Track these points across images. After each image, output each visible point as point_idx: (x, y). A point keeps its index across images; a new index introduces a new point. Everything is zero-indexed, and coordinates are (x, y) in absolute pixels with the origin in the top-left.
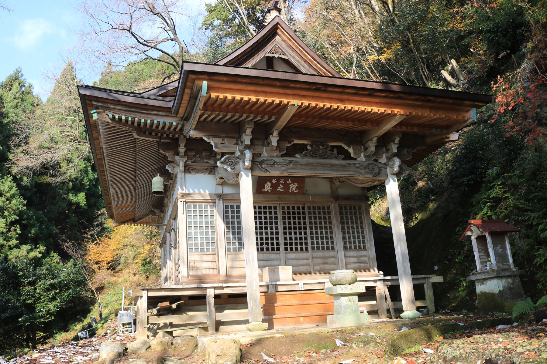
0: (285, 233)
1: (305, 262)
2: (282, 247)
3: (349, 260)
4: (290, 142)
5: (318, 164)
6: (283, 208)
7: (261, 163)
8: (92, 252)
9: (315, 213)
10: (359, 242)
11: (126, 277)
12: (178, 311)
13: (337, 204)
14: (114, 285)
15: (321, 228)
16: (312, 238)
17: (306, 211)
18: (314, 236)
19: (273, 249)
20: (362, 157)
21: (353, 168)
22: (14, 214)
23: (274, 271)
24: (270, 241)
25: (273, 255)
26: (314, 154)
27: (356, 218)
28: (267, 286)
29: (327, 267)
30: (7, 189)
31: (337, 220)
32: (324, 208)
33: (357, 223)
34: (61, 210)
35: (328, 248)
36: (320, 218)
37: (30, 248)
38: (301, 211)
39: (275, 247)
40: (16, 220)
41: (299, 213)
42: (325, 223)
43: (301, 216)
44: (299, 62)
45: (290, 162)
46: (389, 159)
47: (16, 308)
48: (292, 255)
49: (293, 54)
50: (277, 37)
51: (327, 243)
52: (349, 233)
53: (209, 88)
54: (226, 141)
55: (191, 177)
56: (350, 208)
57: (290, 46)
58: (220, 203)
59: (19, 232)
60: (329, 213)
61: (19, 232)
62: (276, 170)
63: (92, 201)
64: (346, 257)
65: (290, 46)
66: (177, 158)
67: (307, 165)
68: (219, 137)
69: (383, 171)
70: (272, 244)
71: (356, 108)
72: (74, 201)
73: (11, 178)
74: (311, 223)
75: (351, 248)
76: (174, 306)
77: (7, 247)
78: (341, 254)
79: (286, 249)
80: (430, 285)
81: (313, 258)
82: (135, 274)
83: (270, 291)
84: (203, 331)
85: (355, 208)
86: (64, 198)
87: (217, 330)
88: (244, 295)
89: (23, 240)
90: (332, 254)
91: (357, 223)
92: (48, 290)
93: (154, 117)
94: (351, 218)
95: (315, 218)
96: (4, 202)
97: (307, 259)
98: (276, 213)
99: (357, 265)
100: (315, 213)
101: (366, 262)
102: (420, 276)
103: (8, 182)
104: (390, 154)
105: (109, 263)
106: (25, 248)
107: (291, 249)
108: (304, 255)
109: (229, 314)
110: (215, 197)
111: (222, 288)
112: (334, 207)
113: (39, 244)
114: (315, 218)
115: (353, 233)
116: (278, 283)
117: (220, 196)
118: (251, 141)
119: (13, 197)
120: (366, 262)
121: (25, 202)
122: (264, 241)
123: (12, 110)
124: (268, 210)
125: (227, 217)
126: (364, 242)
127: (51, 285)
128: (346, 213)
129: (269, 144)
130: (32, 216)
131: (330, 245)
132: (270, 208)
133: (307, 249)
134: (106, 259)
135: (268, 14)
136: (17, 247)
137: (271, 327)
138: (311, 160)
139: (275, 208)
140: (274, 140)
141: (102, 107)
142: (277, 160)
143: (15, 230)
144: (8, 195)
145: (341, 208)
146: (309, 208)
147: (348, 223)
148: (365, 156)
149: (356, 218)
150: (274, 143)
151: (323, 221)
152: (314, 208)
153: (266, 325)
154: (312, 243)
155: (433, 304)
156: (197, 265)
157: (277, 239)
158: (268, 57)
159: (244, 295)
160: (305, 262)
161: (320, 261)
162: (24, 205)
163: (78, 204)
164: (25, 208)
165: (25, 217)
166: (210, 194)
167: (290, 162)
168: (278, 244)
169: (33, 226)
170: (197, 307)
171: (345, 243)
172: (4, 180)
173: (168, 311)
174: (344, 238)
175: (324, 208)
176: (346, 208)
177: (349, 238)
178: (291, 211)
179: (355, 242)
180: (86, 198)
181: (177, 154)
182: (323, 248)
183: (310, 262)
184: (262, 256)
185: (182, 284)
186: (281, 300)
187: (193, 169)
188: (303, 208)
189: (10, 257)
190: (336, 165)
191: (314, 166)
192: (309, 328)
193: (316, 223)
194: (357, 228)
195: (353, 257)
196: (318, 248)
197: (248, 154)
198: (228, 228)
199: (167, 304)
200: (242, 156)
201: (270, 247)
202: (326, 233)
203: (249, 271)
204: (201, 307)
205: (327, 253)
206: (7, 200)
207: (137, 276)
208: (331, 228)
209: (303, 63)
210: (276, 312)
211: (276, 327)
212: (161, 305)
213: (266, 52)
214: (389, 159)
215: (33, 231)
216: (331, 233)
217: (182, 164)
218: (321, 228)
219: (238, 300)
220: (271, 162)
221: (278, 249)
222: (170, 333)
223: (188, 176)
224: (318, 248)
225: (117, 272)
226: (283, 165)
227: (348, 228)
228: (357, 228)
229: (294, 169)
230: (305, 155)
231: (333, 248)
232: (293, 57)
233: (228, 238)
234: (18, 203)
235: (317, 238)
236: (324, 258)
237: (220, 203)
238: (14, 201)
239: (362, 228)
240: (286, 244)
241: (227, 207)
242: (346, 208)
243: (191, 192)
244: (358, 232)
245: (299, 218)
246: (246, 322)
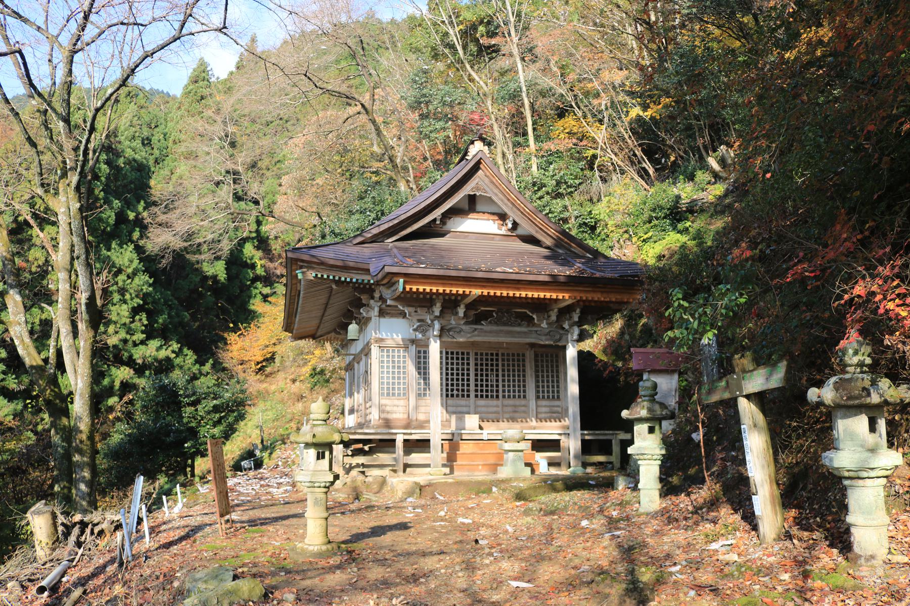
0: (476, 380)
1: (495, 409)
2: (472, 394)
3: (540, 410)
4: (476, 310)
5: (501, 331)
6: (476, 354)
7: (449, 330)
8: (235, 348)
9: (508, 360)
10: (553, 392)
11: (282, 384)
12: (371, 452)
13: (533, 352)
14: (263, 395)
15: (514, 376)
16: (504, 386)
17: (500, 358)
18: (506, 383)
19: (463, 396)
20: (544, 325)
21: (534, 335)
22: (137, 296)
23: (461, 420)
24: (460, 388)
25: (462, 402)
26: (498, 322)
27: (552, 366)
28: (453, 434)
29: (516, 415)
30: (127, 264)
31: (531, 368)
32: (518, 355)
33: (552, 371)
34: (192, 286)
35: (519, 397)
36: (514, 365)
37: (159, 344)
38: (495, 357)
39: (466, 393)
40: (139, 305)
41: (492, 360)
42: (519, 371)
43: (495, 363)
44: (502, 201)
45: (476, 329)
46: (571, 326)
47: (178, 431)
48: (482, 402)
49: (496, 191)
50: (480, 172)
51: (519, 391)
52: (543, 382)
53: (405, 282)
54: (419, 309)
55: (386, 321)
56: (547, 356)
57: (492, 182)
58: (413, 349)
59: (146, 322)
60: (524, 360)
61: (146, 322)
62: (461, 337)
63: (234, 271)
64: (537, 406)
65: (492, 182)
66: (372, 302)
67: (491, 332)
68: (413, 306)
69: (564, 337)
70: (463, 390)
71: (530, 294)
72: (209, 274)
73: (132, 246)
74: (503, 370)
75: (543, 397)
76: (366, 448)
77: (130, 343)
78: (532, 403)
79: (476, 396)
80: (618, 442)
81: (503, 406)
82: (294, 381)
83: (455, 439)
84: (392, 473)
85: (552, 356)
86: (197, 269)
87: (404, 471)
88: (429, 440)
89: (150, 333)
90: (523, 402)
91: (552, 371)
92: (209, 413)
93: (353, 275)
94: (547, 366)
95: (508, 365)
96: (124, 281)
97: (497, 406)
98: (468, 359)
99: (549, 415)
100: (508, 360)
101: (558, 412)
102: (607, 432)
103: (128, 253)
104: (571, 322)
105: (258, 363)
106: (154, 344)
107: (482, 396)
108: (494, 402)
109: (416, 457)
110: (408, 342)
111: (411, 434)
112: (529, 355)
113: (171, 340)
114: (508, 365)
115: (548, 382)
116: (463, 432)
117: (413, 341)
118: (441, 312)
119: (135, 273)
120: (558, 412)
121: (151, 281)
122: (455, 388)
123: (128, 143)
124: (460, 356)
125: (419, 363)
126: (558, 392)
127: (215, 407)
128: (542, 361)
129: (457, 313)
130: (159, 299)
131: (522, 394)
132: (463, 354)
133: (497, 397)
134: (253, 358)
135: (471, 146)
136: (143, 342)
137: (452, 472)
138: (495, 328)
139: (468, 354)
140: (461, 311)
141: (306, 267)
142: (464, 327)
143: (141, 320)
144: (130, 271)
145: (536, 355)
146: (503, 355)
147: (543, 371)
148: (547, 324)
149: (552, 366)
150: (461, 314)
151: (516, 368)
152: (508, 355)
153: (447, 470)
154: (504, 391)
155: (619, 460)
156: (388, 409)
157: (468, 385)
158: (469, 195)
159: (429, 440)
160: (495, 409)
161: (510, 409)
162: (150, 285)
163: (215, 277)
164: (151, 289)
165: (150, 300)
166: (403, 340)
167: (476, 329)
168: (468, 391)
169: (161, 312)
170: (387, 449)
171: (538, 392)
172: (122, 250)
173: (360, 452)
174: (537, 387)
175: (518, 355)
176: (542, 356)
177: (543, 387)
178: (484, 357)
179: (548, 392)
180: (226, 269)
181: (373, 298)
182: (514, 397)
183: (500, 409)
184: (451, 401)
185: (373, 428)
186: (465, 448)
187: (388, 314)
188: (497, 355)
189: (135, 356)
190: (519, 333)
191: (497, 333)
192: (481, 475)
193: (509, 371)
194: (553, 376)
195: (545, 406)
196: (509, 397)
197: (437, 326)
198: (419, 373)
199: (360, 446)
200: (432, 326)
201: (460, 393)
202: (519, 381)
203: (436, 420)
204: (391, 449)
205: (517, 402)
206: (129, 277)
207: (297, 383)
208: (524, 376)
209: (506, 201)
210: (458, 459)
211: (456, 473)
212: (354, 447)
213: (467, 190)
214: (571, 326)
215: (161, 321)
216: (524, 381)
217: (377, 309)
218: (514, 376)
219: (423, 445)
220: (458, 330)
221: (468, 396)
222: (363, 473)
223: (382, 320)
224: (509, 397)
225: (267, 376)
226: (469, 333)
227: (543, 376)
228: (553, 376)
229: (478, 336)
230: (490, 322)
231: (525, 397)
232: (496, 195)
233: (419, 384)
234: (142, 282)
235: (509, 386)
236: (515, 406)
237: (413, 349)
238: (137, 280)
239: (558, 377)
240: (476, 391)
241: (419, 352)
242: (542, 356)
243: (384, 336)
244: (553, 382)
245: (492, 365)
246: (428, 466)
